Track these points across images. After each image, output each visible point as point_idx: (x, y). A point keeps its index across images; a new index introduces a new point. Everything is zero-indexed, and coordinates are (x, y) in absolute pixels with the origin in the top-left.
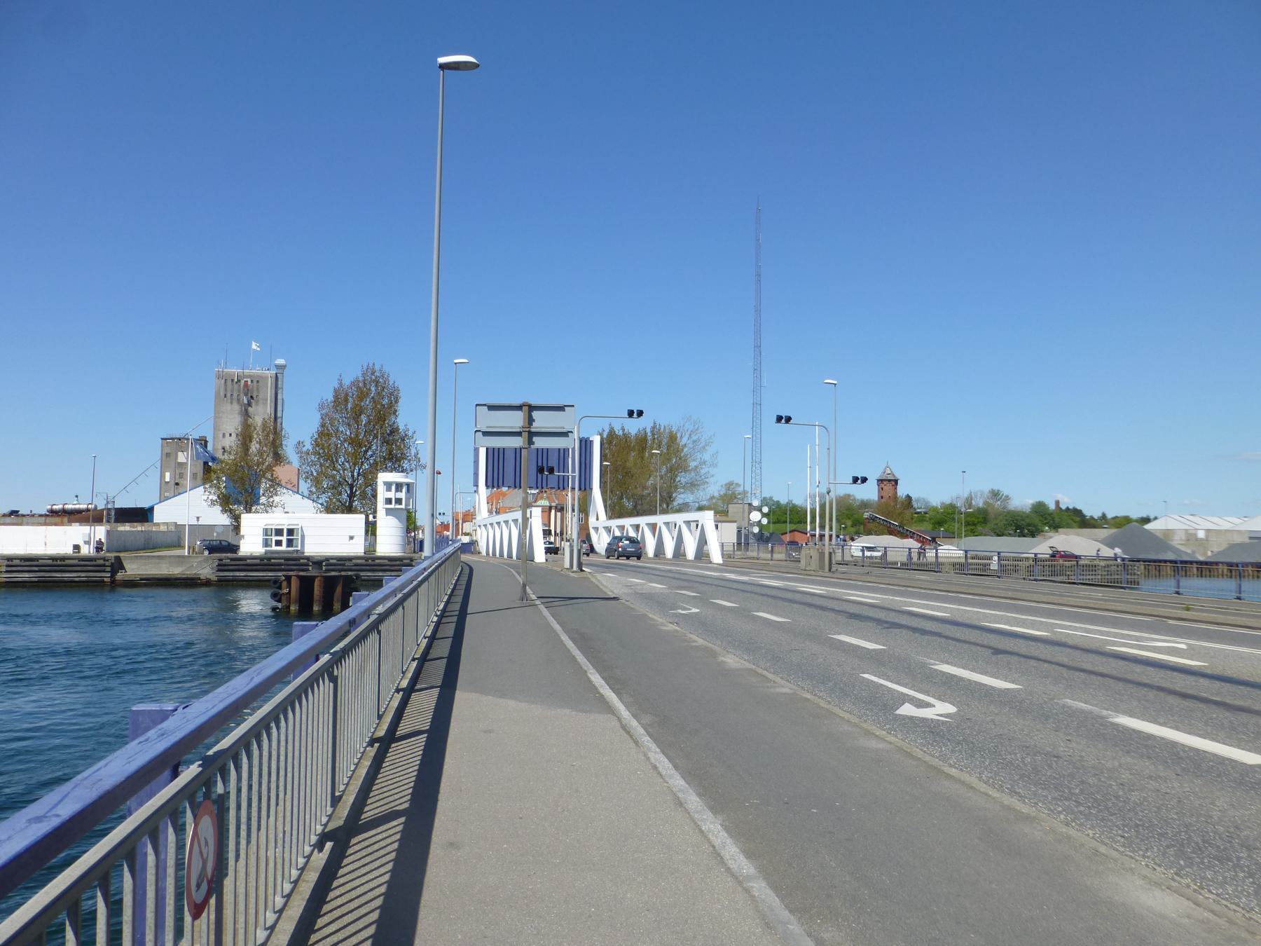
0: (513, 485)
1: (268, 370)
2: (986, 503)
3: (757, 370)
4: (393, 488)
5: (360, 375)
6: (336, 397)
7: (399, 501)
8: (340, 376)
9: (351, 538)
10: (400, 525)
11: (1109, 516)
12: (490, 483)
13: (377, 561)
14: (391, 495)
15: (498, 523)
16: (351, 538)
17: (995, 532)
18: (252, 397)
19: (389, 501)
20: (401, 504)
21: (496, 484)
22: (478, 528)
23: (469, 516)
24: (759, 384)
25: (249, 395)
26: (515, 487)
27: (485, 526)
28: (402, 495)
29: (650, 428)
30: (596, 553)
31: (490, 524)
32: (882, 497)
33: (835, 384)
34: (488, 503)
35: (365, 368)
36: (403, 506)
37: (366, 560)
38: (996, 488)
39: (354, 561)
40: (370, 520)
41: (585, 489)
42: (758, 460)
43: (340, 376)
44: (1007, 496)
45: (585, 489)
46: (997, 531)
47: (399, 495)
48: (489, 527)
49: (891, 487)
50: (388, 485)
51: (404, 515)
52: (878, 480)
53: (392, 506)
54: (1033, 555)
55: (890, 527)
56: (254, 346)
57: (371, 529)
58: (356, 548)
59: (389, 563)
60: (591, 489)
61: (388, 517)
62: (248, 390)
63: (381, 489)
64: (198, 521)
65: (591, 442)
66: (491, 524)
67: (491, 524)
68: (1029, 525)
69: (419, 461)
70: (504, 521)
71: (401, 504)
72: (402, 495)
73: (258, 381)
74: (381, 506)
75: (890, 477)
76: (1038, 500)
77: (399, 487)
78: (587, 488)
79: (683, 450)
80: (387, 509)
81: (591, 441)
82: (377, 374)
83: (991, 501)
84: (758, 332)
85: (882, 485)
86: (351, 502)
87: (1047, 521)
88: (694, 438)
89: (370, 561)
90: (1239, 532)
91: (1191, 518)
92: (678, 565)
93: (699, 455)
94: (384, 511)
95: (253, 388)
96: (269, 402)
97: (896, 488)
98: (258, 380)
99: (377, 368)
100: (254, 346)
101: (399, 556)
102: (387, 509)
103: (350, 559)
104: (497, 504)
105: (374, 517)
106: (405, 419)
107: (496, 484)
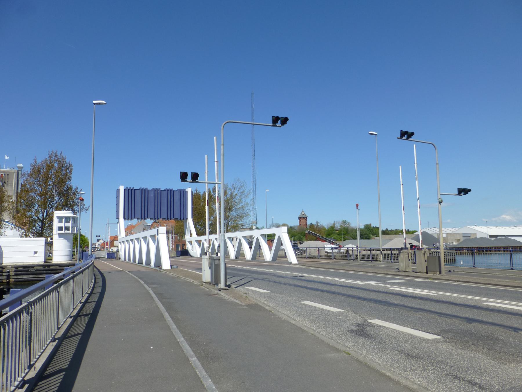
0: (140, 217)
1: (14, 169)
2: (341, 226)
3: (253, 167)
4: (64, 220)
5: (47, 157)
6: (33, 170)
7: (67, 228)
8: (35, 157)
9: (35, 253)
10: (68, 243)
11: (389, 229)
12: (126, 217)
13: (51, 267)
14: (62, 225)
15: (132, 240)
16: (35, 253)
17: (352, 238)
18: (5, 182)
19: (60, 229)
20: (69, 230)
21: (130, 217)
22: (119, 244)
23: (114, 239)
24: (254, 173)
25: (3, 181)
26: (142, 219)
27: (123, 242)
28: (70, 225)
29: (212, 188)
30: (190, 256)
31: (131, 240)
32: (301, 224)
33: (376, 135)
34: (125, 231)
35: (51, 153)
36: (70, 232)
37: (43, 267)
38: (344, 220)
39: (35, 268)
40: (49, 241)
41: (183, 219)
42: (255, 208)
43: (35, 157)
44: (349, 223)
45: (183, 219)
46: (353, 237)
47: (67, 225)
48: (126, 243)
49: (304, 220)
50: (60, 219)
51: (71, 237)
52: (299, 217)
53: (63, 232)
54: (351, 249)
55: (317, 237)
56: (6, 157)
57: (49, 245)
58: (39, 259)
59: (60, 268)
60: (187, 219)
61: (60, 239)
62: (3, 179)
63: (55, 220)
64: (188, 241)
65: (186, 192)
66: (127, 241)
67: (127, 241)
68: (365, 234)
69: (84, 206)
70: (143, 238)
71: (69, 230)
72: (70, 225)
73: (8, 175)
74: (55, 232)
75: (304, 216)
76: (366, 224)
77: (67, 219)
78: (185, 219)
79: (235, 197)
80: (59, 234)
81: (186, 191)
82: (59, 157)
83: (342, 225)
84: (254, 149)
85: (301, 219)
86: (42, 231)
87: (371, 232)
88: (241, 191)
89: (46, 267)
90: (459, 234)
91: (434, 229)
92: (279, 268)
93: (243, 200)
94: (57, 235)
95: (5, 178)
96: (14, 184)
97: (306, 221)
98: (8, 174)
99: (59, 153)
100: (6, 157)
101: (66, 263)
102: (59, 234)
103: (32, 267)
104: (130, 232)
105: (52, 239)
106: (75, 182)
107: (130, 217)
